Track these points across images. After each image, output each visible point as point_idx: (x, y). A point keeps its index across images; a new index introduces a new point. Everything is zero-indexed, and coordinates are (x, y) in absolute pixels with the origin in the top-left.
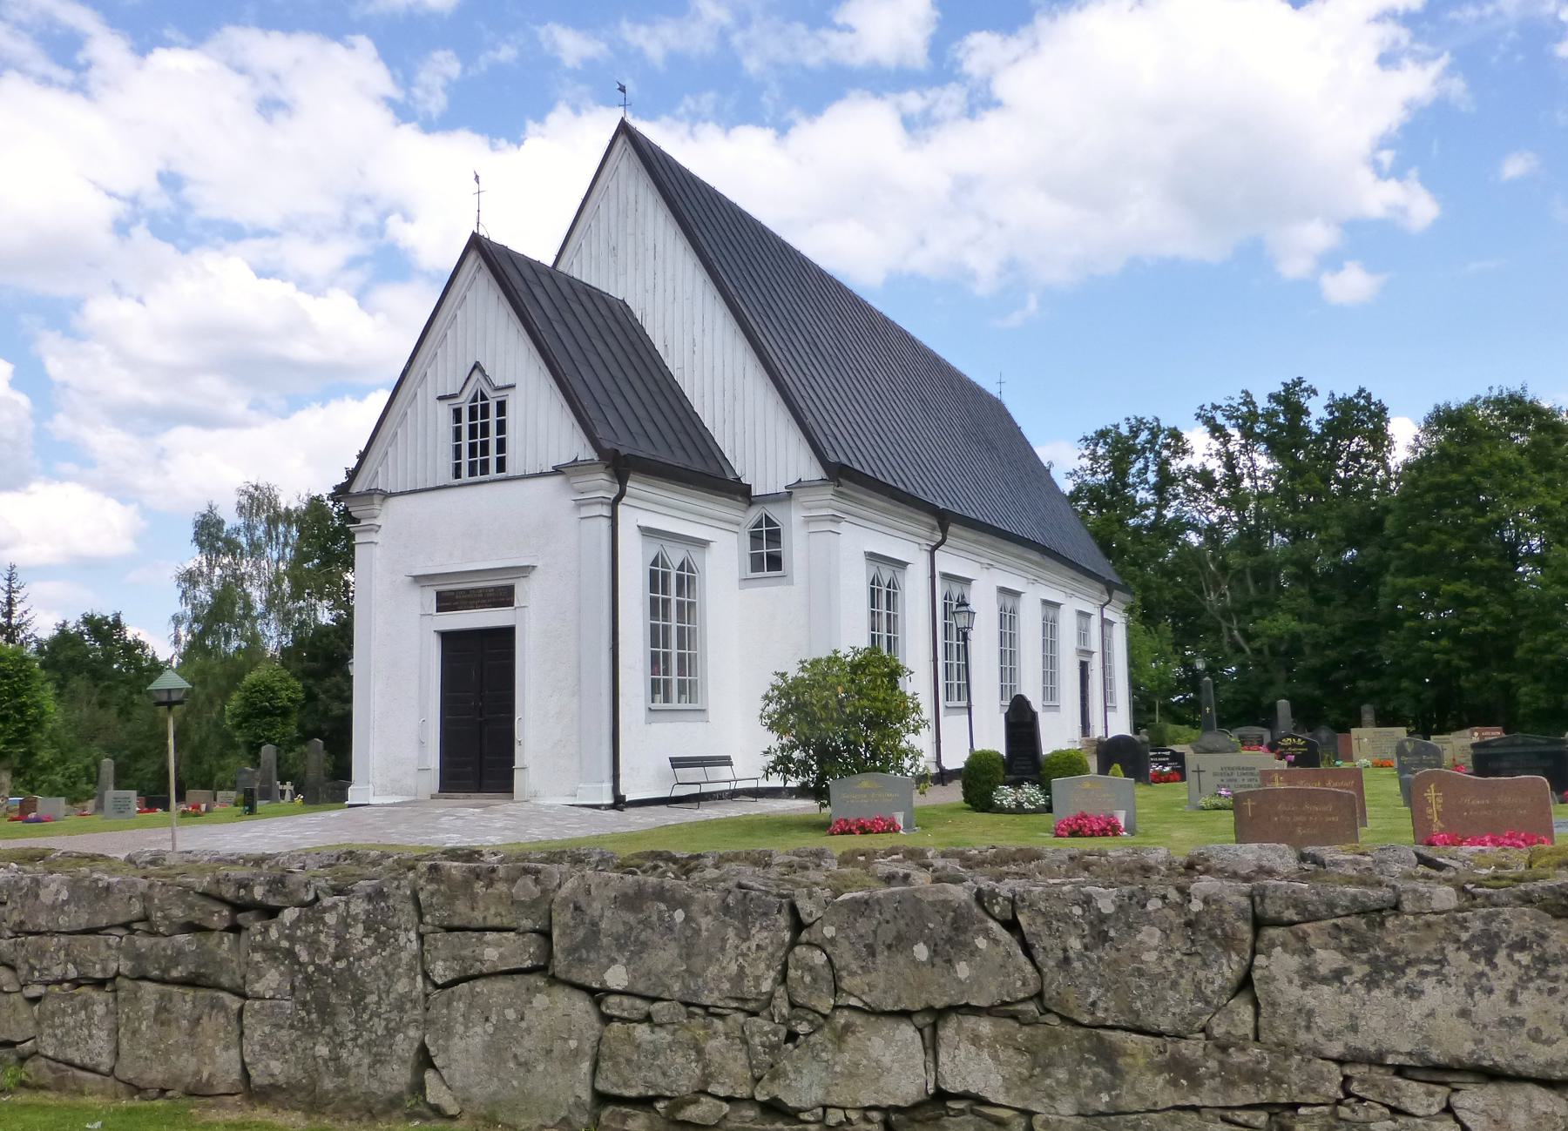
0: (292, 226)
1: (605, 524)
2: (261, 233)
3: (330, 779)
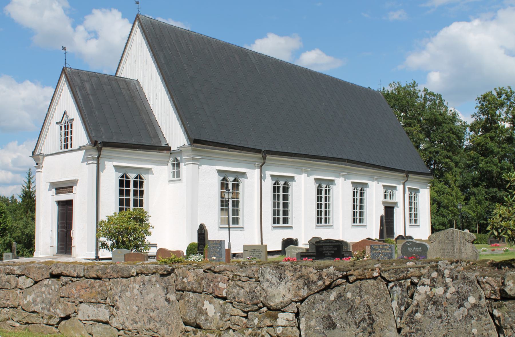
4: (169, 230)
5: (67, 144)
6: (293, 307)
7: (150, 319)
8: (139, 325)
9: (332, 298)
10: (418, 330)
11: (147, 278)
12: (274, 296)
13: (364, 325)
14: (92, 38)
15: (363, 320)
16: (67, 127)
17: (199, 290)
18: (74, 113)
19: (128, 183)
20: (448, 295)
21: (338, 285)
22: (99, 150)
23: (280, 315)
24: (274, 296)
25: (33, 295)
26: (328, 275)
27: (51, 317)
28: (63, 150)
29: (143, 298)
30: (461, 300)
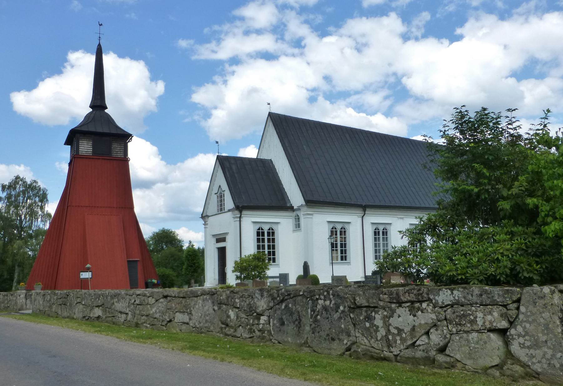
0: (367, 88)
1: (238, 223)
2: (357, 93)
3: (200, 281)
4: (287, 265)
5: (221, 209)
6: (267, 313)
7: (206, 321)
8: (202, 324)
9: (283, 307)
10: (318, 326)
11: (205, 297)
12: (259, 307)
13: (297, 323)
14: (357, 93)
15: (296, 320)
16: (221, 197)
17: (227, 303)
18: (225, 187)
19: (263, 234)
20: (331, 305)
21: (286, 300)
22: (241, 212)
23: (262, 317)
24: (259, 307)
25: (155, 308)
26: (282, 294)
27: (163, 321)
28: (219, 212)
29: (203, 308)
30: (337, 307)
